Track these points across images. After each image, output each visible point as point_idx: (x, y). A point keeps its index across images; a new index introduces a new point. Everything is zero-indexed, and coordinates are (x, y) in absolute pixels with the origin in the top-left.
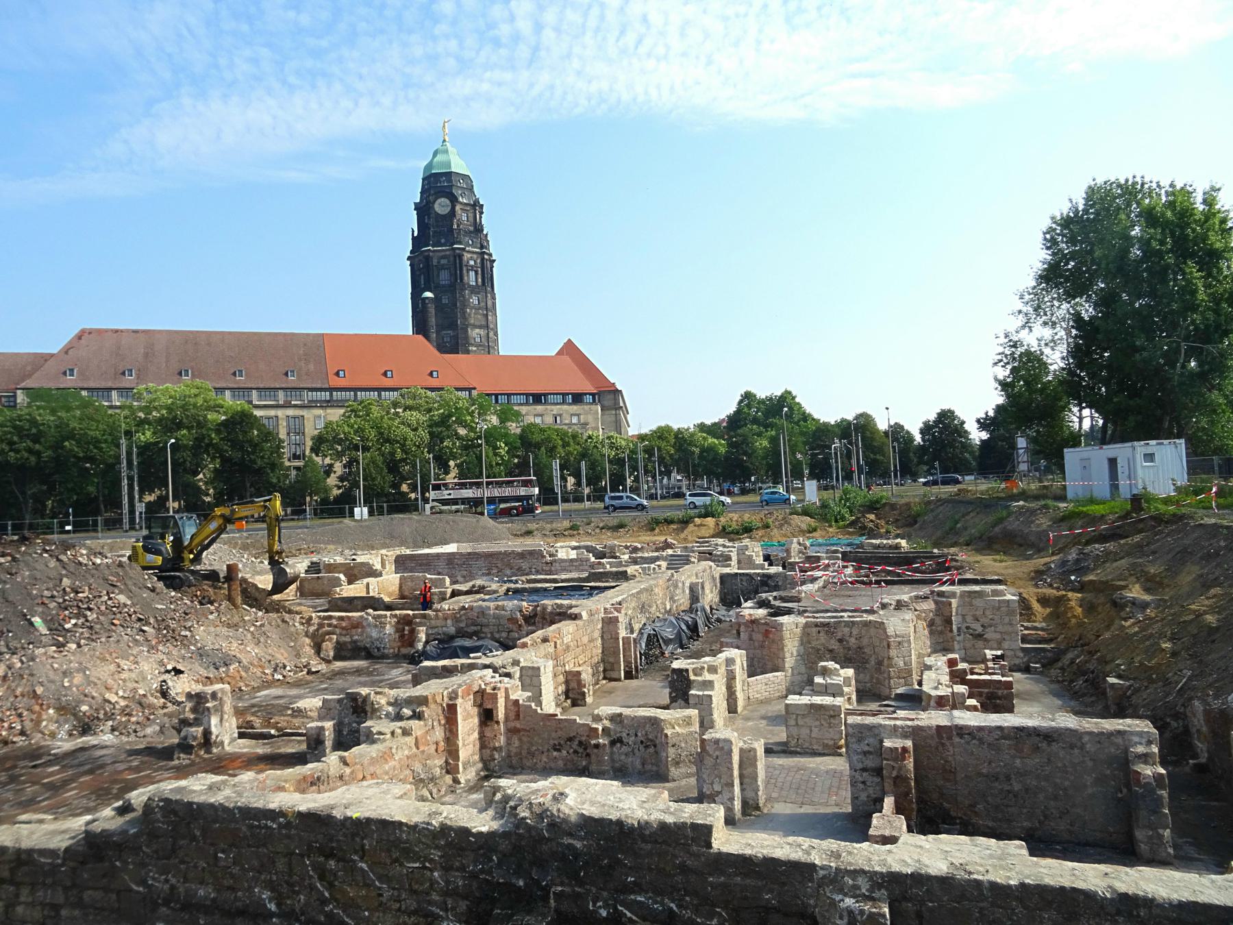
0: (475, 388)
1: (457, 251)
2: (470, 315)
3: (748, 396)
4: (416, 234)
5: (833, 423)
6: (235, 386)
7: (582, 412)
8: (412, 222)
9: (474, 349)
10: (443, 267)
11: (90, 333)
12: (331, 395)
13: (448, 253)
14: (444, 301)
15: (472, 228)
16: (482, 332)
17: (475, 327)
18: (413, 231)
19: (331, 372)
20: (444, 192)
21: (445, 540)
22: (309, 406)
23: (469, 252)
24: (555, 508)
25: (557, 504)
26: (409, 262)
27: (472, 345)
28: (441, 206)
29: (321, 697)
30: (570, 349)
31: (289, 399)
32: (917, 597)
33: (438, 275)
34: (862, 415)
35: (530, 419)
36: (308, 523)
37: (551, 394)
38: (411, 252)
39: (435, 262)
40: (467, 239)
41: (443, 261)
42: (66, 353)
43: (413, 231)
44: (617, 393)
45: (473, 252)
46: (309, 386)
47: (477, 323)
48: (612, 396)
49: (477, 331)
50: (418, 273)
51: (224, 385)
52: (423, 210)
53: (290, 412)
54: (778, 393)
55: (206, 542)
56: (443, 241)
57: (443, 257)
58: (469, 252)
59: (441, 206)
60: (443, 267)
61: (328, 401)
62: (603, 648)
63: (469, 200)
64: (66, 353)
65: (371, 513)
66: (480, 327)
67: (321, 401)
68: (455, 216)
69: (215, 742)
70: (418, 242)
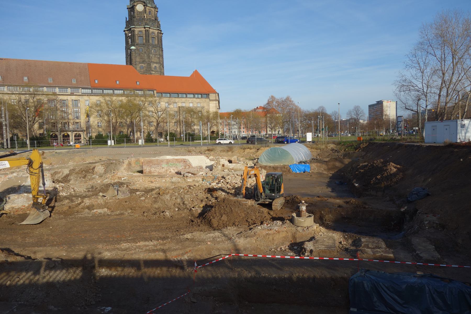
1: (146, 28)
3: (272, 97)
4: (128, 20)
6: (48, 85)
7: (202, 102)
9: (154, 72)
12: (92, 91)
15: (153, 19)
16: (157, 66)
17: (154, 63)
18: (126, 18)
21: (381, 109)
22: (83, 95)
24: (200, 141)
25: (200, 140)
31: (73, 92)
34: (321, 107)
35: (180, 105)
36: (435, 122)
37: (245, 143)
43: (126, 18)
47: (155, 61)
49: (155, 65)
51: (43, 85)
53: (74, 98)
54: (285, 97)
61: (91, 94)
66: (156, 63)
68: (145, 12)
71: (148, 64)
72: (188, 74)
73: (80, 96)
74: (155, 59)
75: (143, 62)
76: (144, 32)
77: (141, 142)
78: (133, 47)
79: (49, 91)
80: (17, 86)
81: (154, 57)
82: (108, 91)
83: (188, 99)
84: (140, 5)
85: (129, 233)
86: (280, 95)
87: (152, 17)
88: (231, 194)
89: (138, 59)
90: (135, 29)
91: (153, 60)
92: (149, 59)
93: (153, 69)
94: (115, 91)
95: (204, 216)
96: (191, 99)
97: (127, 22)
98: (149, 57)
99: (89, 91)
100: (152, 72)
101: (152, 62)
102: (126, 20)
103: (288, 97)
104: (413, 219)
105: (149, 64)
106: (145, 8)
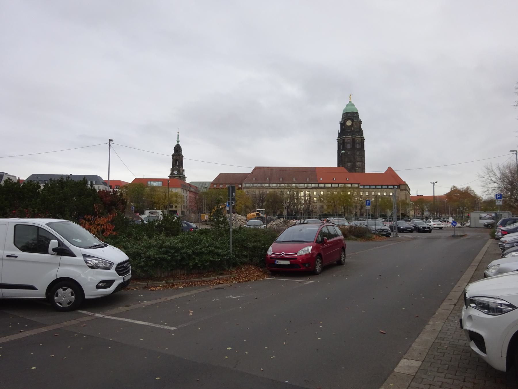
0: (359, 184)
1: (353, 138)
4: (339, 132)
5: (360, 119)
8: (338, 128)
9: (358, 169)
10: (349, 143)
11: (257, 168)
13: (350, 138)
16: (360, 163)
18: (339, 131)
26: (337, 141)
27: (357, 167)
28: (349, 123)
29: (73, 303)
32: (101, 245)
37: (383, 185)
38: (338, 138)
39: (346, 141)
41: (349, 141)
42: (252, 173)
43: (339, 131)
44: (405, 185)
48: (404, 186)
49: (359, 163)
50: (340, 144)
52: (343, 124)
58: (357, 137)
60: (349, 143)
62: (458, 282)
63: (358, 120)
64: (252, 173)
66: (360, 162)
67: (315, 187)
70: (340, 134)
72: (383, 170)
73: (311, 189)
74: (358, 159)
75: (350, 162)
78: (343, 152)
79: (268, 186)
82: (328, 185)
83: (383, 190)
86: (461, 186)
88: (445, 369)
90: (345, 139)
94: (279, 184)
95: (415, 226)
96: (386, 189)
97: (339, 133)
99: (317, 185)
100: (356, 169)
102: (339, 132)
103: (468, 187)
104: (468, 221)
105: (355, 163)
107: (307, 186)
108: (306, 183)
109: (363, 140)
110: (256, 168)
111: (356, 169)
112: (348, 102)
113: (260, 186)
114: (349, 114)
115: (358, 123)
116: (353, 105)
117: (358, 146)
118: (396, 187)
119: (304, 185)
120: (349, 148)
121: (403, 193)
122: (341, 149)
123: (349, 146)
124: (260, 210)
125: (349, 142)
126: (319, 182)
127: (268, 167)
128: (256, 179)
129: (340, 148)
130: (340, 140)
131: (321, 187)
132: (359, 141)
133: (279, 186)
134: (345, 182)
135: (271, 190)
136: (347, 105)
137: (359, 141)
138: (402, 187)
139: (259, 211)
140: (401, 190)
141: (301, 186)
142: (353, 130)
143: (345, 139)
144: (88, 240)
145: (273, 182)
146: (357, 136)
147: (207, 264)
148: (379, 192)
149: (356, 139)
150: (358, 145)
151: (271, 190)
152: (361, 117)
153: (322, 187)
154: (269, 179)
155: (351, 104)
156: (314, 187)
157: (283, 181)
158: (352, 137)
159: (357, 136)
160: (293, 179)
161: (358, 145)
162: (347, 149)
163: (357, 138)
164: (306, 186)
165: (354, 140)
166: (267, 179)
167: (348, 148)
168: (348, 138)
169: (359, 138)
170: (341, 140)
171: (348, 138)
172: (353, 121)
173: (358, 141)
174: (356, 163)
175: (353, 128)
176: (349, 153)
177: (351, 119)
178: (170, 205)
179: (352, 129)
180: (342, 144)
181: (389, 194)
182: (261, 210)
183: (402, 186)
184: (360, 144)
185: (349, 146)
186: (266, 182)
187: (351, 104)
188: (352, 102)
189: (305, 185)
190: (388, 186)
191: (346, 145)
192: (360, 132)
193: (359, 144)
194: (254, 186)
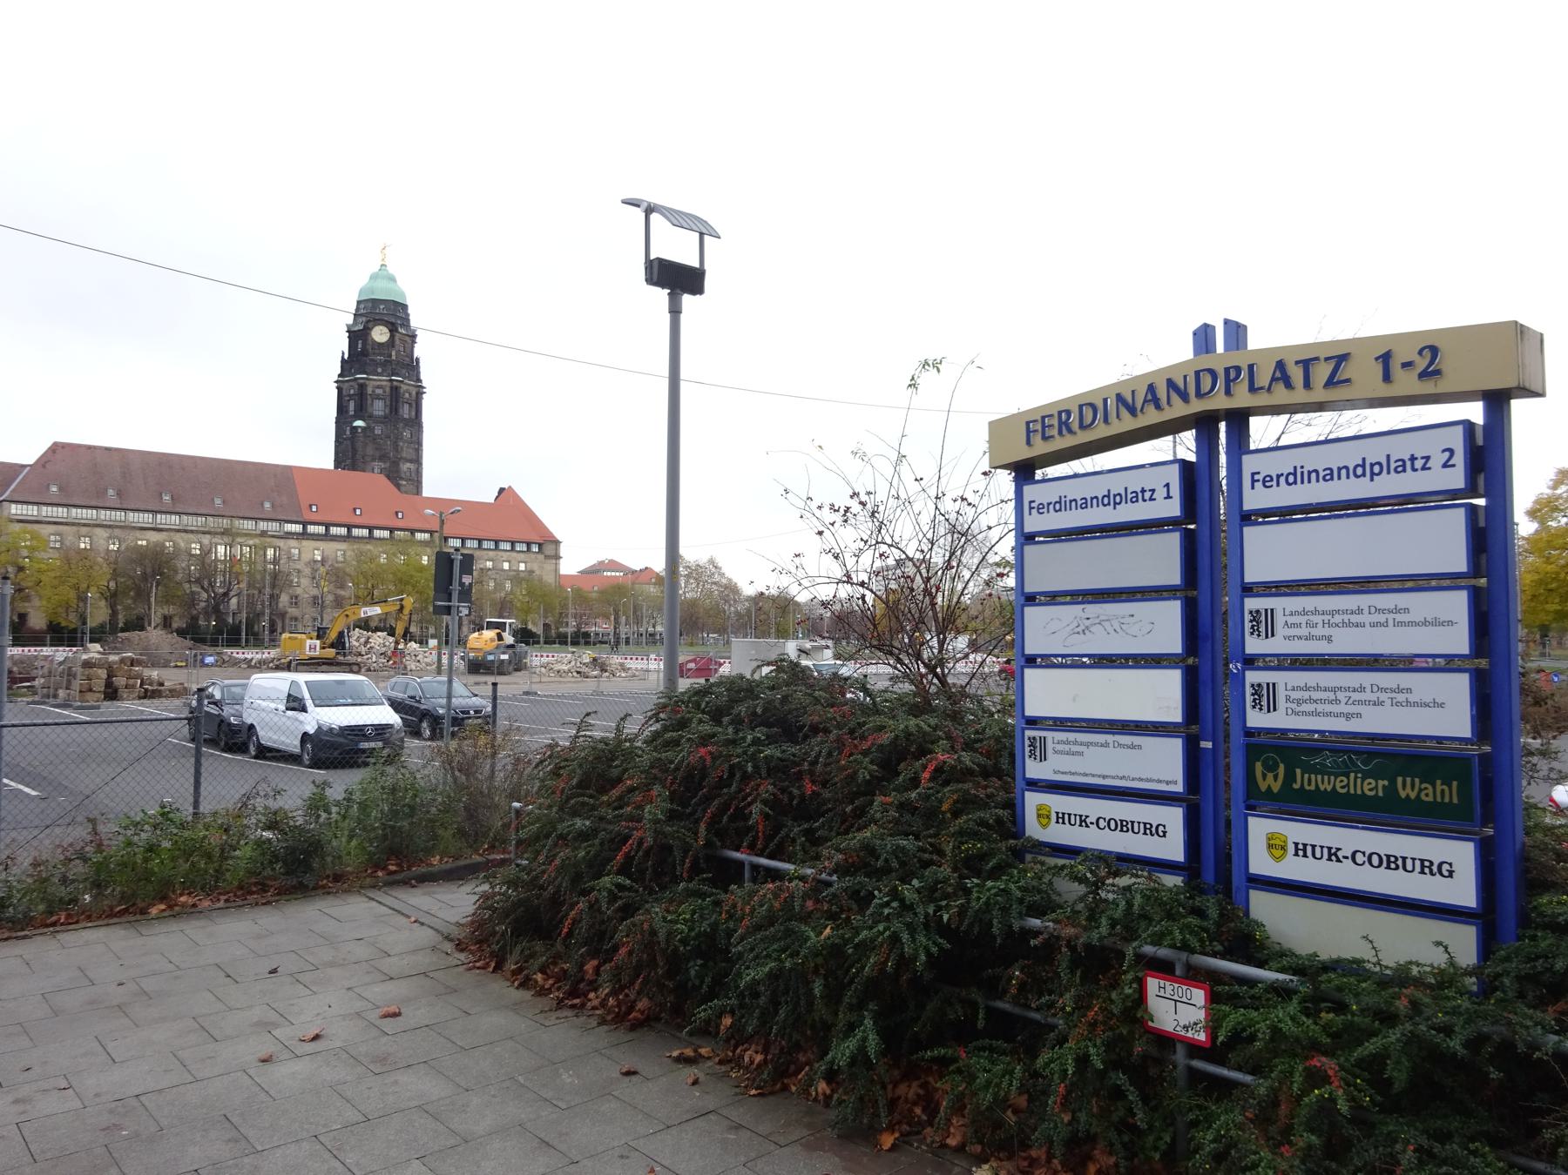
1: (395, 383)
2: (402, 448)
4: (346, 356)
8: (343, 345)
9: (404, 483)
14: (376, 432)
18: (343, 353)
19: (304, 505)
20: (383, 320)
23: (406, 384)
27: (402, 479)
30: (712, 561)
33: (372, 404)
38: (339, 376)
39: (369, 390)
40: (404, 371)
41: (379, 391)
43: (343, 353)
45: (409, 385)
46: (285, 518)
47: (409, 457)
48: (554, 547)
49: (408, 465)
52: (357, 336)
55: (1068, 598)
56: (380, 370)
57: (378, 387)
58: (406, 384)
59: (380, 334)
60: (378, 397)
64: (44, 466)
65: (1226, 595)
66: (411, 461)
68: (393, 346)
69: (1012, 568)
70: (348, 366)
71: (394, 462)
74: (407, 452)
76: (388, 389)
77: (1195, 593)
78: (359, 423)
79: (190, 524)
80: (171, 513)
81: (407, 447)
84: (381, 327)
85: (692, 581)
87: (1011, 1073)
89: (370, 450)
90: (367, 382)
91: (404, 455)
92: (397, 451)
93: (403, 476)
94: (159, 516)
98: (396, 448)
100: (401, 482)
101: (401, 458)
102: (343, 357)
106: (392, 336)
107: (265, 529)
108: (260, 516)
109: (420, 392)
110: (56, 448)
111: (401, 482)
112: (376, 269)
113: (113, 518)
114: (382, 307)
115: (407, 338)
116: (392, 279)
117: (405, 411)
118: (535, 548)
119: (65, 510)
120: (381, 413)
121: (549, 566)
122: (352, 413)
123: (379, 408)
124: (505, 623)
125: (379, 395)
126: (308, 516)
127: (108, 449)
128: (61, 489)
129: (347, 412)
130: (345, 386)
131: (314, 534)
132: (410, 394)
133: (158, 521)
134: (391, 524)
135: (155, 537)
136: (374, 277)
137: (410, 394)
138: (549, 549)
139: (501, 626)
140: (547, 557)
141: (55, 515)
142: (394, 358)
143: (367, 382)
144: (868, 777)
145: (133, 507)
146: (406, 381)
147: (868, 834)
148: (489, 560)
149: (404, 387)
150: (406, 407)
151: (155, 537)
152: (415, 321)
153: (318, 535)
154: (119, 494)
155: (383, 274)
156: (290, 533)
157: (174, 504)
158: (391, 380)
159: (406, 381)
160: (213, 500)
161: (406, 407)
162: (371, 416)
163: (407, 388)
164: (261, 528)
165: (395, 390)
166: (111, 492)
167: (376, 413)
168: (378, 382)
169: (411, 388)
170: (351, 383)
171: (379, 383)
172: (393, 330)
173: (407, 395)
174: (401, 465)
175: (393, 353)
176: (378, 431)
177: (387, 321)
178: (323, 607)
179: (391, 356)
180: (351, 401)
181: (515, 568)
182: (508, 621)
183: (547, 545)
184: (414, 405)
185: (379, 408)
186: (107, 505)
187: (383, 274)
188: (391, 270)
189: (154, 519)
190: (480, 541)
191: (369, 402)
192: (411, 367)
193: (410, 404)
194: (115, 521)
